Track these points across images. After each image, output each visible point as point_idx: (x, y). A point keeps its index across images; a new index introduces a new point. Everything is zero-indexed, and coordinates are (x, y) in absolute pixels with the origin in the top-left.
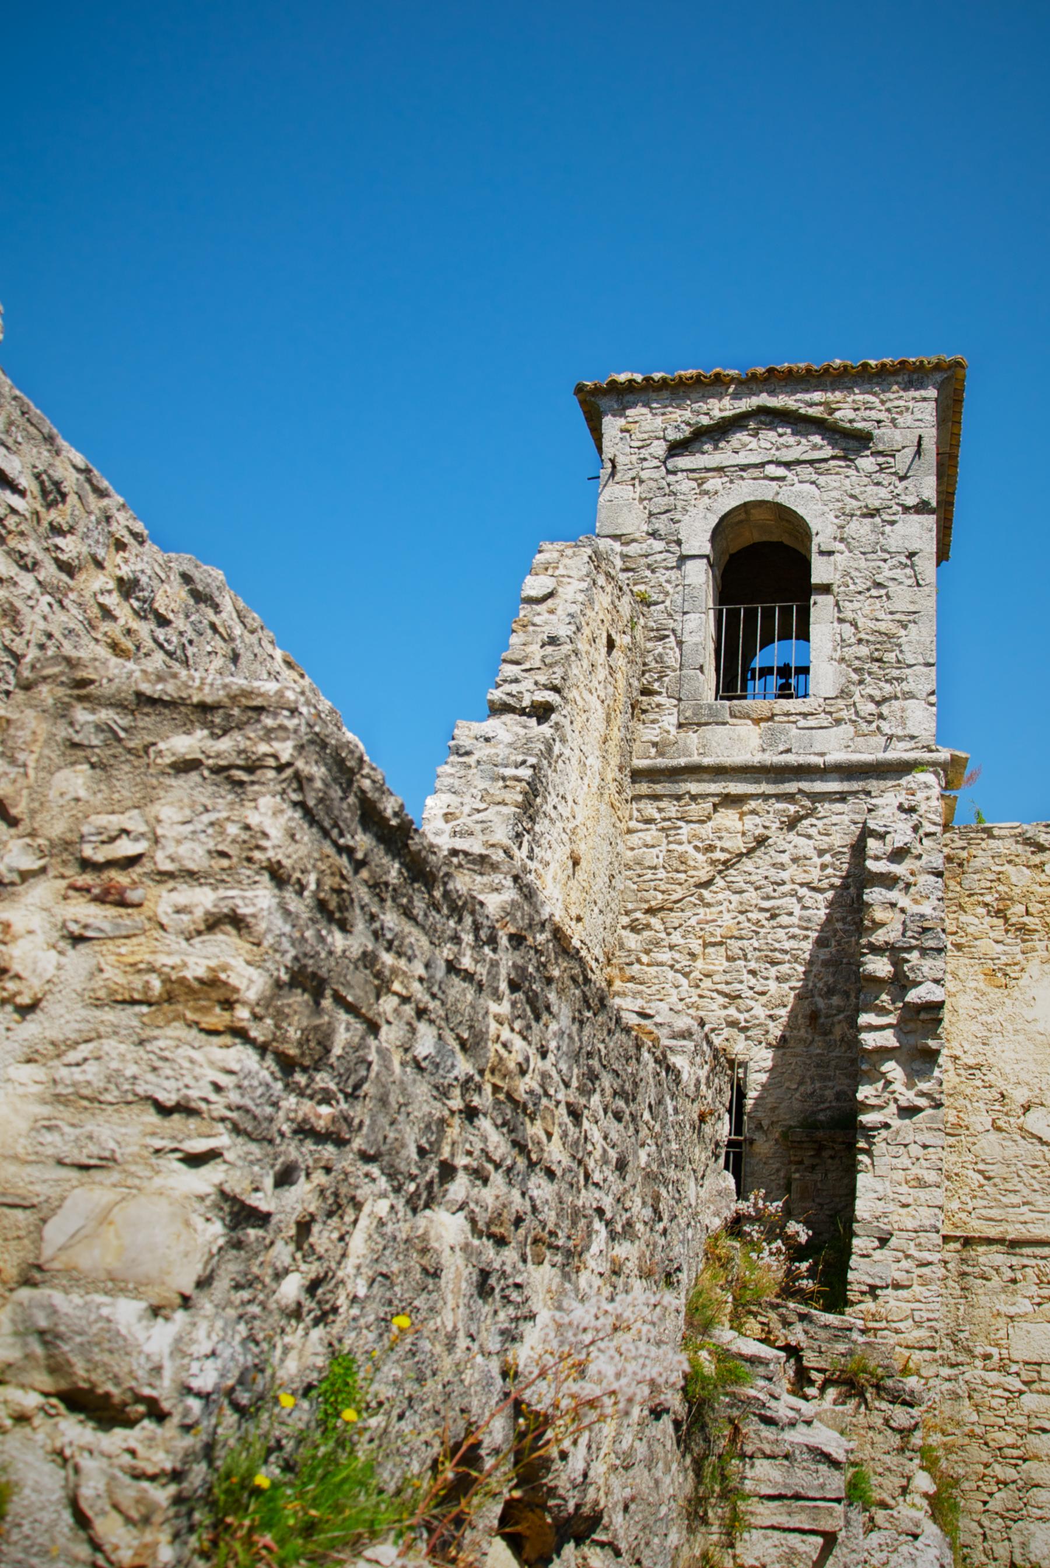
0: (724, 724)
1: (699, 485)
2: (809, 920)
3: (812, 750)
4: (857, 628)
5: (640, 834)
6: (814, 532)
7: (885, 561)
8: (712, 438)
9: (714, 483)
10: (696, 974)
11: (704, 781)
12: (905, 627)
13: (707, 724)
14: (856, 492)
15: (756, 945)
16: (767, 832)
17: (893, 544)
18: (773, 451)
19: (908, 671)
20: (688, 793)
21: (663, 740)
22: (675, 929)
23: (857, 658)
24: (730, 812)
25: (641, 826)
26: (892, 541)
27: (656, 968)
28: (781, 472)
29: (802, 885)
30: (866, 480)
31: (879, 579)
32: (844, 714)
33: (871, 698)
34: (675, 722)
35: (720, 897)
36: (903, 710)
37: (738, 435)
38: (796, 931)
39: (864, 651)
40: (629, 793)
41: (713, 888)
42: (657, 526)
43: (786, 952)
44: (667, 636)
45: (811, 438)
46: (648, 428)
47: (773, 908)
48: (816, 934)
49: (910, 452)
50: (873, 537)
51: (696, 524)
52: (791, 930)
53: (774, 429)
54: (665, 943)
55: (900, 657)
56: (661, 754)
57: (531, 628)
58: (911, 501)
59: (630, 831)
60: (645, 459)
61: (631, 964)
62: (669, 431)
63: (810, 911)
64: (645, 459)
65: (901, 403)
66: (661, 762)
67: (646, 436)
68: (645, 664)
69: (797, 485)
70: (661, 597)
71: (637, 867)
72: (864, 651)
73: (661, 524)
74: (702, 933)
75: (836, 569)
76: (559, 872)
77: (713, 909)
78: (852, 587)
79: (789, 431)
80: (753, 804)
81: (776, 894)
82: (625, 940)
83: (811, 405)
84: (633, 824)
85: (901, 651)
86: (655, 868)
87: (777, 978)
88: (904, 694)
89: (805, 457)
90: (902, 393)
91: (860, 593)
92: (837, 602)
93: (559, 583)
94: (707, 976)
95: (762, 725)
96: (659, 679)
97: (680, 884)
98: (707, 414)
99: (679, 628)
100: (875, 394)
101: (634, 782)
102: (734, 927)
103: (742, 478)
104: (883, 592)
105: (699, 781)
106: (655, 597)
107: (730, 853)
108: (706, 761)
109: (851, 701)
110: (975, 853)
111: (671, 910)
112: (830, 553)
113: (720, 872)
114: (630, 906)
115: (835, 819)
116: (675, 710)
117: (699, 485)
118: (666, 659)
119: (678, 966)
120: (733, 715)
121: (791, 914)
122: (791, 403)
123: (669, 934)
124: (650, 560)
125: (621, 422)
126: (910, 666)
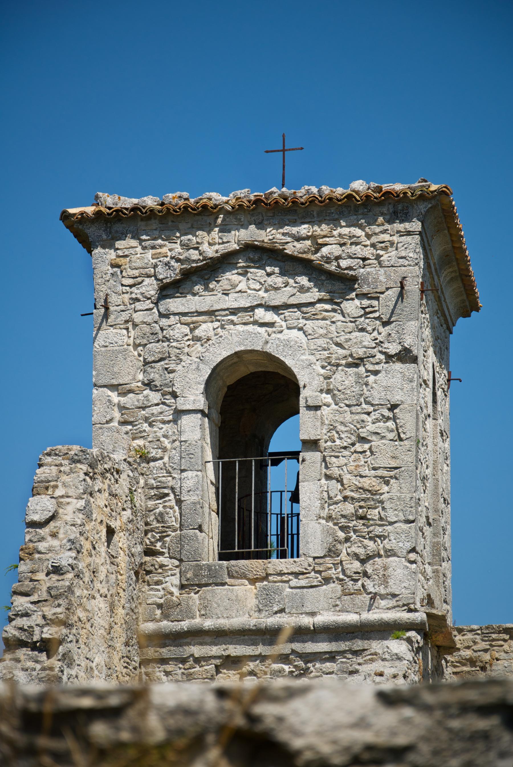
0: (223, 584)
1: (192, 330)
4: (342, 485)
6: (301, 384)
7: (368, 414)
8: (202, 277)
12: (387, 483)
13: (207, 585)
14: (341, 339)
17: (376, 396)
18: (261, 293)
19: (389, 528)
20: (192, 655)
21: (167, 601)
23: (343, 516)
26: (375, 393)
28: (270, 316)
32: (332, 573)
33: (356, 556)
36: (385, 568)
37: (228, 275)
39: (349, 508)
42: (152, 376)
44: (167, 495)
45: (299, 279)
46: (138, 264)
49: (393, 293)
50: (357, 389)
51: (190, 376)
53: (262, 267)
55: (383, 514)
56: (166, 616)
57: (37, 556)
58: (393, 349)
60: (137, 300)
62: (159, 269)
64: (137, 300)
65: (386, 237)
66: (166, 625)
67: (136, 273)
68: (147, 524)
69: (286, 331)
72: (349, 508)
75: (323, 423)
78: (338, 442)
79: (277, 270)
80: (251, 665)
83: (299, 239)
85: (384, 509)
88: (386, 551)
89: (293, 301)
90: (387, 226)
91: (345, 448)
92: (324, 457)
93: (59, 505)
95: (258, 584)
96: (161, 539)
98: (197, 249)
99: (177, 486)
103: (232, 323)
104: (367, 446)
105: (201, 644)
106: (153, 453)
108: (208, 624)
110: (497, 655)
112: (317, 408)
116: (178, 570)
117: (192, 330)
118: (166, 518)
120: (231, 576)
122: (279, 236)
125: (111, 255)
126: (391, 523)
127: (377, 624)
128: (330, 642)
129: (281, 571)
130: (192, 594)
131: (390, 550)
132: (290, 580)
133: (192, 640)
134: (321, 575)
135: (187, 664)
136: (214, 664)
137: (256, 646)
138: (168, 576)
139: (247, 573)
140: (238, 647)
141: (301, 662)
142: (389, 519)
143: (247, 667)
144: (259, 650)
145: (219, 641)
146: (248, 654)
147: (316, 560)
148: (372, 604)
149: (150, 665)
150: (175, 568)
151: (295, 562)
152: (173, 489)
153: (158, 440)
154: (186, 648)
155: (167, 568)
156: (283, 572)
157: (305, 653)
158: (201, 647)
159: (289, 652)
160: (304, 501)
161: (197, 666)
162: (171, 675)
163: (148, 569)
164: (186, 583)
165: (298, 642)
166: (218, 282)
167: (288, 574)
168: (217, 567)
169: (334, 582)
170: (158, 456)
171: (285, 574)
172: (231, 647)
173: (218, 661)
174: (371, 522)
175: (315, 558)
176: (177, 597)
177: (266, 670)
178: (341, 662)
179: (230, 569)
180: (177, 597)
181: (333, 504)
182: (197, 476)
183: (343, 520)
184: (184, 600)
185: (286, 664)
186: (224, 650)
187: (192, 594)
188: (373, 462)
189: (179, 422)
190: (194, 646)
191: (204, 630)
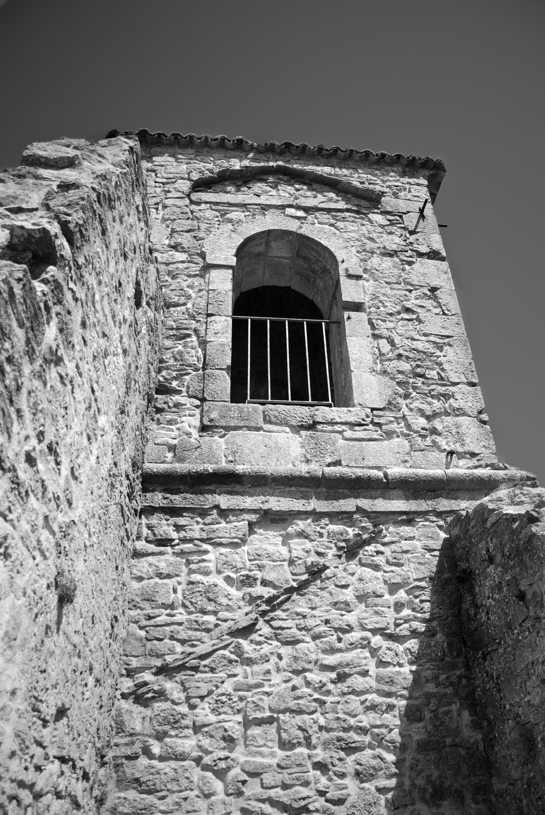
0: (258, 429)
2: (391, 682)
3: (365, 463)
5: (150, 559)
6: (339, 259)
9: (237, 214)
10: (235, 772)
11: (237, 493)
14: (374, 235)
15: (322, 721)
16: (322, 561)
20: (217, 507)
22: (202, 698)
23: (400, 372)
24: (271, 533)
25: (152, 548)
27: (173, 764)
29: (374, 631)
30: (380, 230)
31: (408, 305)
32: (394, 426)
34: (198, 424)
35: (266, 649)
38: (373, 697)
39: (405, 366)
40: (139, 503)
41: (255, 637)
42: (179, 240)
43: (363, 731)
47: (340, 665)
48: (404, 702)
50: (396, 271)
52: (370, 697)
53: (292, 185)
54: (187, 722)
59: (137, 554)
61: (133, 757)
63: (390, 669)
67: (171, 176)
68: (161, 361)
70: (183, 300)
71: (146, 605)
73: (185, 240)
74: (242, 705)
76: (26, 620)
77: (256, 668)
80: (301, 525)
81: (341, 645)
82: (126, 717)
84: (141, 545)
86: (172, 606)
87: (358, 774)
91: (391, 314)
94: (253, 775)
97: (208, 631)
99: (202, 329)
100: (375, 175)
101: (145, 490)
102: (289, 694)
105: (230, 493)
107: (275, 587)
109: (400, 415)
111: (195, 669)
113: (264, 614)
114: (135, 663)
115: (405, 545)
116: (198, 411)
117: (222, 215)
118: (187, 357)
119: (207, 760)
121: (365, 674)
123: (192, 707)
124: (171, 267)
127: (468, 479)
128: (408, 500)
129: (332, 419)
130: (216, 438)
131: (458, 409)
132: (344, 431)
133: (217, 488)
134: (381, 429)
135: (209, 517)
136: (248, 520)
137: (308, 500)
138: (185, 416)
139: (289, 419)
140: (282, 499)
141: (368, 524)
142: (451, 380)
143: (295, 527)
144: (312, 505)
145: (256, 492)
146: (296, 509)
147: (375, 412)
148: (450, 462)
149: (155, 516)
150: (194, 408)
151: (349, 411)
152: (195, 330)
153: (182, 290)
154: (209, 496)
155: (184, 407)
156: (335, 421)
157: (376, 512)
158: (229, 497)
159: (354, 509)
160: (353, 353)
161: (223, 521)
162: (184, 530)
163: (159, 406)
164: (209, 424)
165: (364, 497)
166: (249, 188)
167: (342, 423)
168: (251, 410)
169: (398, 437)
170: (181, 302)
171: (337, 423)
172: (272, 499)
173: (253, 516)
174: (430, 382)
175: (373, 409)
176: (196, 439)
177: (322, 531)
178: (423, 525)
179: (266, 413)
180: (196, 439)
181: (387, 360)
182: (226, 320)
183: (399, 376)
184: (205, 443)
185: (350, 526)
186: (263, 503)
187: (216, 438)
188: (422, 329)
189: (208, 275)
190: (219, 494)
191: (237, 474)
